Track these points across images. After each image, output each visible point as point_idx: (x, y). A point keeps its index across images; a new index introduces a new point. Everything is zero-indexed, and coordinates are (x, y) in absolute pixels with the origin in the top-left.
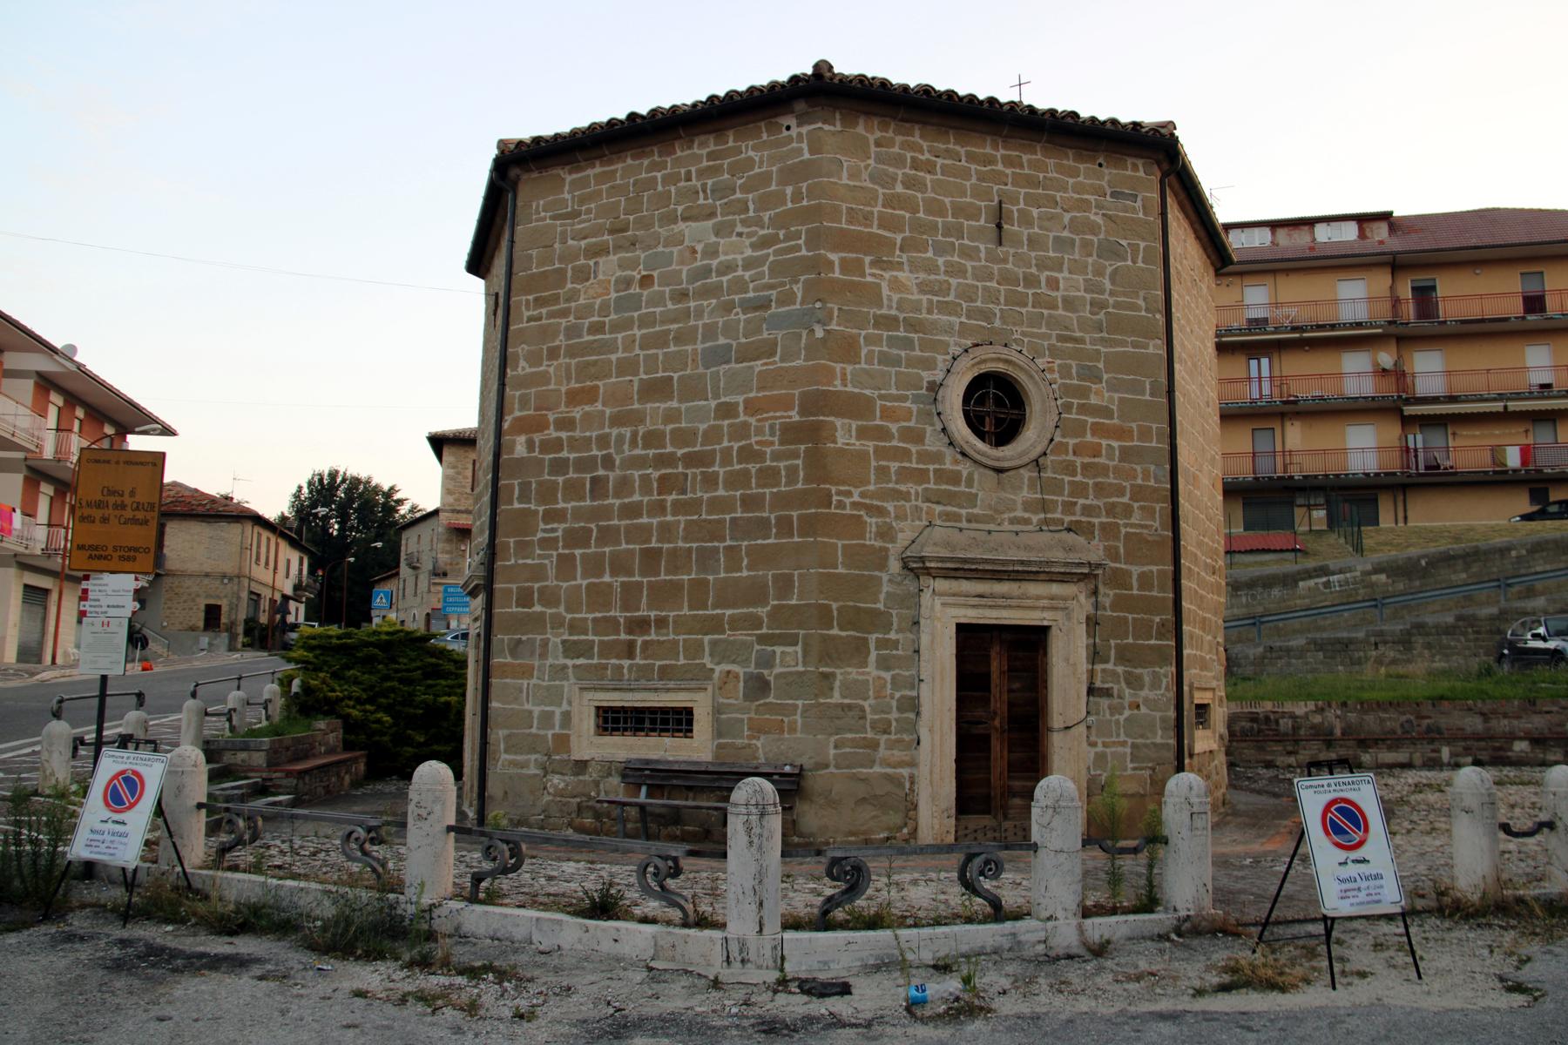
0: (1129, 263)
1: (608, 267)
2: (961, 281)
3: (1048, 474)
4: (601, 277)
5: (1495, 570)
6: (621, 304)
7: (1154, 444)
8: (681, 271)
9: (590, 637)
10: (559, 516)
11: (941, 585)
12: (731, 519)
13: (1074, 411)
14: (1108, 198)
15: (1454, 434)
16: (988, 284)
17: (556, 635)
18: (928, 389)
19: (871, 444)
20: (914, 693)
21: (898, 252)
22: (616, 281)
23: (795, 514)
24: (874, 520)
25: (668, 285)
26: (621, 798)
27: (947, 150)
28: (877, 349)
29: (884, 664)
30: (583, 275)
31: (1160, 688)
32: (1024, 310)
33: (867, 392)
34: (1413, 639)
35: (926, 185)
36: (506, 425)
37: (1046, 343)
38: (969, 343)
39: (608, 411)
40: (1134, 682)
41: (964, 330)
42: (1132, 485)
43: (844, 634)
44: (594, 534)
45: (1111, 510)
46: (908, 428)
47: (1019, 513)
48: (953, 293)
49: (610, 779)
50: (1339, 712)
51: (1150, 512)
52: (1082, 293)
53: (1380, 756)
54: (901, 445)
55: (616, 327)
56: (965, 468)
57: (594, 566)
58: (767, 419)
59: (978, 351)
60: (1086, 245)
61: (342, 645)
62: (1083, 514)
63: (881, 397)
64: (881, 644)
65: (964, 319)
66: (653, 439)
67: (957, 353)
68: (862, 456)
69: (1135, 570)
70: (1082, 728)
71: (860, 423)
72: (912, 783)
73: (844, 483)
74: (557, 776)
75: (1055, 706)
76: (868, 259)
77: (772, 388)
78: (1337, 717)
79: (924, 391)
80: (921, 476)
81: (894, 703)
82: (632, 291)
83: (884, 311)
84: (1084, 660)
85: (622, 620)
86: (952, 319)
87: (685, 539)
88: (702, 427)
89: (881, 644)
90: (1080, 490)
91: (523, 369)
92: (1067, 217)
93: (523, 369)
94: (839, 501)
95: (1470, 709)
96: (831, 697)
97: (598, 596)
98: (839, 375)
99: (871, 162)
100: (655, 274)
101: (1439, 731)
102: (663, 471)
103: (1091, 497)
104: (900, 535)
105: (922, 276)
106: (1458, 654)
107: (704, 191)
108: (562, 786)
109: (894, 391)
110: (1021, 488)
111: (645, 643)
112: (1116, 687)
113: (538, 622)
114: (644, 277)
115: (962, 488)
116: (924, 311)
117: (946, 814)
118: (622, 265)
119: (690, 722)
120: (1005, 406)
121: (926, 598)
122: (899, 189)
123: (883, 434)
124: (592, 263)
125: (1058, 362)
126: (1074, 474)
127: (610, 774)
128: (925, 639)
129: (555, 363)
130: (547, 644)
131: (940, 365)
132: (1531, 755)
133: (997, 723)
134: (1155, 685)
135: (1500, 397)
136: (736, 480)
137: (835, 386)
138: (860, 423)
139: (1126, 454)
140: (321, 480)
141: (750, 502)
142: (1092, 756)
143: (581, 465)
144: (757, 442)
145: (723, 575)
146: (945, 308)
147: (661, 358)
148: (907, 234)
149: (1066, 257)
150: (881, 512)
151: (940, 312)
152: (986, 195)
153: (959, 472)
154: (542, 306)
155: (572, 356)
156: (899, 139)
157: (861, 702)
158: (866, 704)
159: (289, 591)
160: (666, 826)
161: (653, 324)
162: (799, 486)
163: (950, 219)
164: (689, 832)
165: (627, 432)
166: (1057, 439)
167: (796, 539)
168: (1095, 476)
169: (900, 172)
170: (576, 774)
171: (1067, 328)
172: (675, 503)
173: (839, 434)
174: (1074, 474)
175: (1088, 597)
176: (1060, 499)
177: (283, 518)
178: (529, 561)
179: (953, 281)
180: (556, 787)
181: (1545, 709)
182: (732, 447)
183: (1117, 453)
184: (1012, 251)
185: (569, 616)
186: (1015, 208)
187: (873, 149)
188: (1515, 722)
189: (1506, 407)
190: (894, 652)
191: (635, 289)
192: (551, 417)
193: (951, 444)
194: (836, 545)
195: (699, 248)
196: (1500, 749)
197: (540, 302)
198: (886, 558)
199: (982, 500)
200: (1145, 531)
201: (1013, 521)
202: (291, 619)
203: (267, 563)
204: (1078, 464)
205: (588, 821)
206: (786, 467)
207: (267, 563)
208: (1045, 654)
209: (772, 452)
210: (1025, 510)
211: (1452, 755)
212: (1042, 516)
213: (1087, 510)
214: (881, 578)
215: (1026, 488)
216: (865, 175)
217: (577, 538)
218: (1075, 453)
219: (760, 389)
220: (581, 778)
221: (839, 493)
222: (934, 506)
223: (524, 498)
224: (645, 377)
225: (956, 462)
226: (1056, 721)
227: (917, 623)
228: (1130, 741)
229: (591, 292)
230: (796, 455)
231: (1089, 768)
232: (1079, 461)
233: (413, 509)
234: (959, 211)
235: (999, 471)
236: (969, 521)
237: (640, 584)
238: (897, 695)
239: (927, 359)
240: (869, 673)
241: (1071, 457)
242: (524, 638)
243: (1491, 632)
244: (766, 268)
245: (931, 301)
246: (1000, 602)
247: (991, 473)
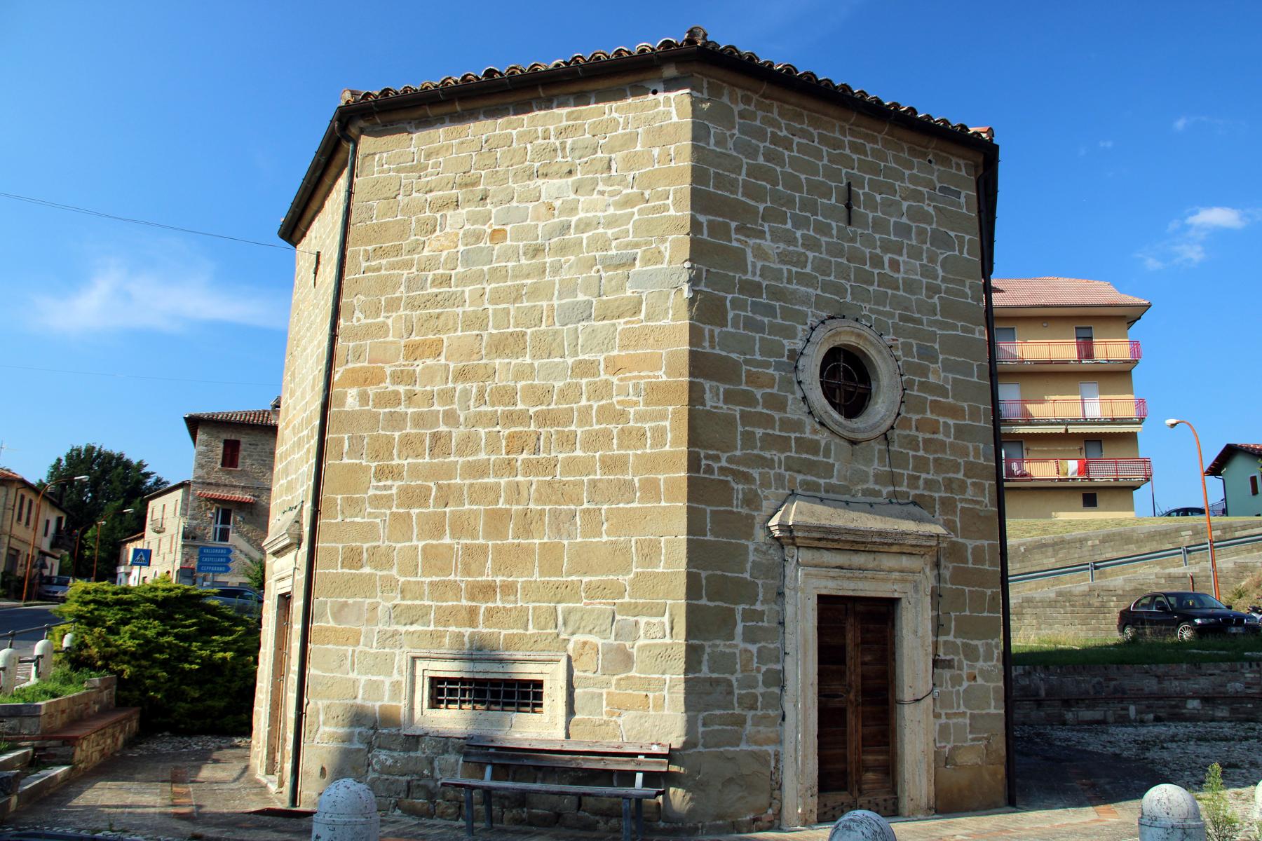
0: (957, 253)
1: (456, 220)
2: (817, 254)
3: (895, 448)
4: (448, 230)
5: (1076, 556)
6: (468, 259)
7: (982, 424)
8: (536, 227)
9: (427, 603)
10: (395, 473)
11: (805, 555)
12: (589, 481)
13: (916, 388)
14: (937, 192)
15: (1027, 449)
16: (839, 260)
17: (386, 600)
18: (788, 357)
19: (738, 408)
20: (779, 667)
21: (760, 221)
22: (464, 234)
23: (661, 477)
24: (740, 487)
25: (522, 240)
26: (459, 779)
27: (802, 130)
28: (743, 313)
29: (750, 636)
30: (430, 228)
31: (992, 660)
32: (871, 289)
33: (734, 356)
34: (1024, 611)
35: (784, 160)
36: (336, 377)
37: (890, 322)
38: (825, 315)
39: (452, 366)
40: (971, 653)
41: (819, 303)
42: (966, 462)
43: (712, 604)
44: (433, 494)
45: (949, 485)
46: (771, 394)
47: (871, 485)
48: (809, 266)
49: (446, 756)
50: (1043, 676)
51: (979, 487)
52: (918, 277)
53: (1080, 714)
54: (765, 411)
55: (464, 280)
56: (823, 437)
57: (435, 527)
58: (630, 379)
59: (834, 323)
60: (921, 232)
61: (118, 600)
62: (924, 489)
63: (747, 362)
64: (748, 615)
65: (819, 292)
66: (506, 395)
67: (814, 324)
68: (729, 421)
69: (970, 544)
70: (929, 700)
71: (727, 386)
72: (777, 761)
73: (711, 447)
74: (384, 752)
75: (905, 678)
76: (733, 225)
77: (636, 347)
78: (1042, 679)
79: (785, 359)
80: (783, 444)
81: (760, 678)
82: (482, 245)
83: (749, 277)
84: (930, 633)
85: (463, 585)
86: (810, 290)
87: (538, 501)
88: (559, 384)
89: (749, 615)
90: (921, 464)
91: (359, 320)
92: (905, 205)
93: (359, 320)
94: (708, 466)
95: (1147, 672)
96: (700, 671)
97: (435, 559)
98: (707, 337)
99: (736, 131)
100: (508, 228)
101: (1124, 692)
102: (513, 429)
103: (932, 472)
104: (765, 503)
105: (782, 246)
106: (1057, 623)
107: (564, 149)
108: (390, 762)
109: (758, 357)
110: (872, 461)
111: (489, 610)
112: (956, 658)
113: (367, 585)
114: (494, 231)
115: (821, 458)
116: (785, 281)
117: (809, 793)
118: (473, 219)
119: (539, 696)
120: (852, 379)
121: (790, 570)
122: (761, 160)
123: (748, 399)
124: (438, 215)
125: (901, 340)
126: (917, 449)
127: (445, 751)
128: (789, 610)
129: (394, 314)
130: (375, 608)
131: (800, 334)
132: (1202, 712)
133: (852, 696)
134: (988, 657)
135: (1063, 422)
136: (593, 441)
137: (704, 348)
138: (727, 386)
139: (960, 431)
140: (79, 455)
141: (610, 464)
142: (937, 727)
143: (420, 420)
144: (618, 402)
145: (579, 540)
146: (803, 279)
147: (512, 313)
148: (769, 204)
149: (905, 241)
150: (747, 478)
151: (798, 283)
152: (835, 175)
153: (818, 442)
154: (381, 257)
155: (413, 308)
156: (760, 114)
157: (727, 676)
158: (733, 679)
159: (46, 547)
160: (510, 809)
161: (505, 278)
162: (667, 448)
163: (805, 195)
164: (537, 816)
165: (474, 387)
166: (903, 414)
167: (663, 504)
168: (936, 452)
169: (761, 145)
170: (407, 750)
171: (906, 309)
172: (527, 463)
173: (708, 396)
174: (917, 449)
175: (931, 570)
176: (905, 472)
177: (42, 484)
178: (358, 520)
179: (810, 255)
180: (382, 764)
181: (1209, 672)
182: (591, 406)
183: (952, 430)
184: (859, 231)
185: (402, 579)
186: (861, 192)
187: (737, 119)
188: (1185, 683)
189: (1067, 430)
190: (760, 624)
191: (485, 244)
192: (388, 370)
193: (810, 413)
194: (705, 510)
195: (557, 204)
196: (1176, 706)
197: (380, 252)
198: (752, 527)
199: (838, 471)
200: (978, 507)
201: (866, 492)
202: (46, 572)
203: (28, 523)
204: (920, 439)
205: (420, 802)
206: (653, 430)
207: (28, 523)
208: (893, 626)
209: (636, 413)
210: (876, 483)
211: (1138, 712)
212: (891, 488)
213: (929, 484)
214: (747, 546)
215: (876, 461)
216: (730, 144)
217: (413, 497)
218: (917, 429)
219: (624, 347)
220: (412, 754)
221: (707, 457)
222: (796, 475)
223: (353, 452)
224: (495, 332)
225: (815, 432)
226: (907, 695)
227: (781, 594)
228: (969, 712)
229: (435, 244)
230: (663, 416)
231: (935, 740)
232: (921, 436)
233: (158, 481)
234: (814, 187)
235: (853, 442)
236: (827, 491)
237: (484, 549)
238: (764, 669)
239: (788, 327)
240: (736, 646)
241: (913, 432)
242: (351, 601)
243: (1084, 606)
244: (630, 226)
245: (789, 271)
246: (857, 573)
247: (846, 444)
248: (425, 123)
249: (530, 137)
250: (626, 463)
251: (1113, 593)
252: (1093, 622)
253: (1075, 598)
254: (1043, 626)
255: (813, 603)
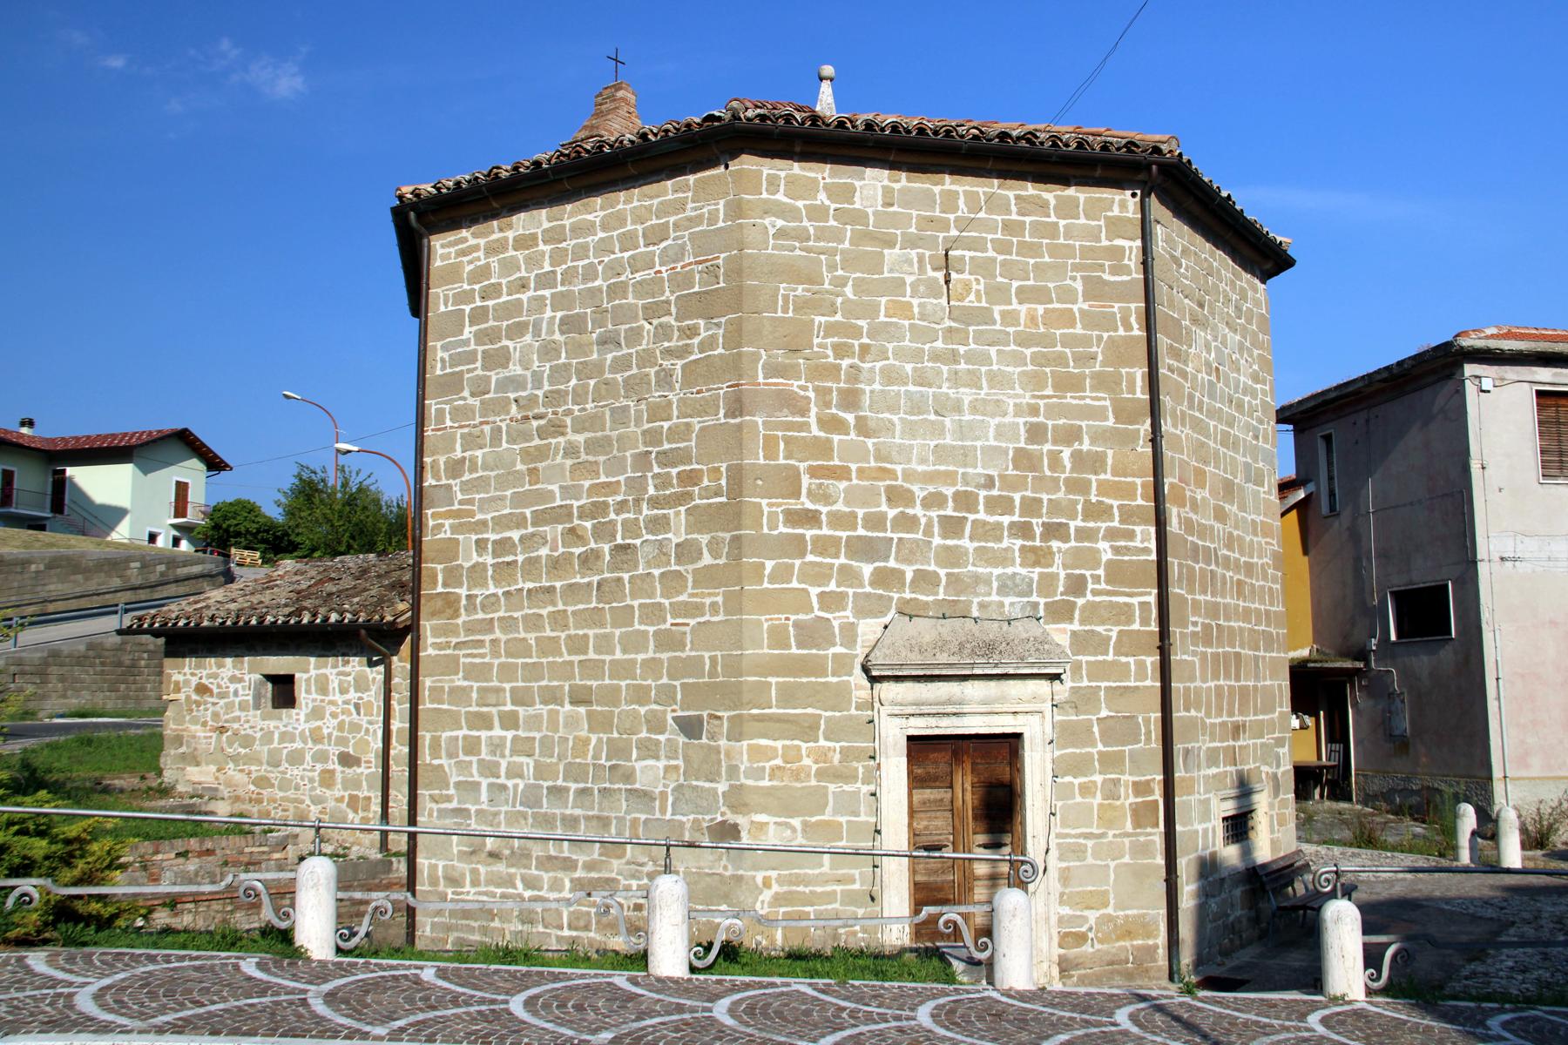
250: (988, 582)
251: (143, 648)
252: (123, 687)
253: (107, 653)
254: (69, 693)
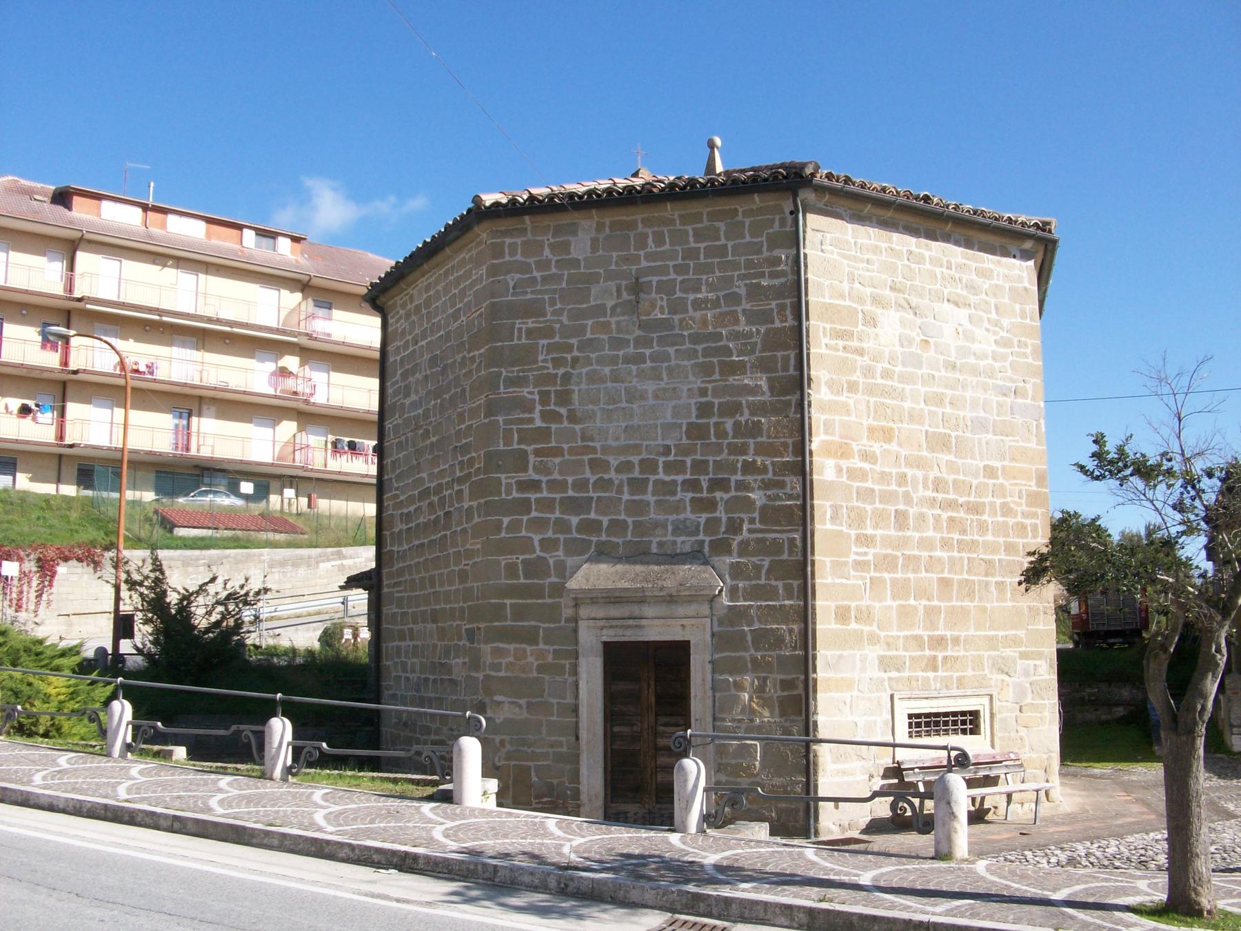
113: (858, 638)
217: (887, 563)
248: (858, 218)
249: (935, 261)
255: (678, 636)
